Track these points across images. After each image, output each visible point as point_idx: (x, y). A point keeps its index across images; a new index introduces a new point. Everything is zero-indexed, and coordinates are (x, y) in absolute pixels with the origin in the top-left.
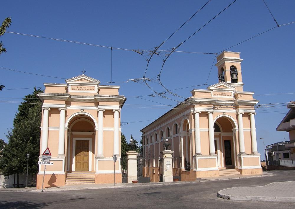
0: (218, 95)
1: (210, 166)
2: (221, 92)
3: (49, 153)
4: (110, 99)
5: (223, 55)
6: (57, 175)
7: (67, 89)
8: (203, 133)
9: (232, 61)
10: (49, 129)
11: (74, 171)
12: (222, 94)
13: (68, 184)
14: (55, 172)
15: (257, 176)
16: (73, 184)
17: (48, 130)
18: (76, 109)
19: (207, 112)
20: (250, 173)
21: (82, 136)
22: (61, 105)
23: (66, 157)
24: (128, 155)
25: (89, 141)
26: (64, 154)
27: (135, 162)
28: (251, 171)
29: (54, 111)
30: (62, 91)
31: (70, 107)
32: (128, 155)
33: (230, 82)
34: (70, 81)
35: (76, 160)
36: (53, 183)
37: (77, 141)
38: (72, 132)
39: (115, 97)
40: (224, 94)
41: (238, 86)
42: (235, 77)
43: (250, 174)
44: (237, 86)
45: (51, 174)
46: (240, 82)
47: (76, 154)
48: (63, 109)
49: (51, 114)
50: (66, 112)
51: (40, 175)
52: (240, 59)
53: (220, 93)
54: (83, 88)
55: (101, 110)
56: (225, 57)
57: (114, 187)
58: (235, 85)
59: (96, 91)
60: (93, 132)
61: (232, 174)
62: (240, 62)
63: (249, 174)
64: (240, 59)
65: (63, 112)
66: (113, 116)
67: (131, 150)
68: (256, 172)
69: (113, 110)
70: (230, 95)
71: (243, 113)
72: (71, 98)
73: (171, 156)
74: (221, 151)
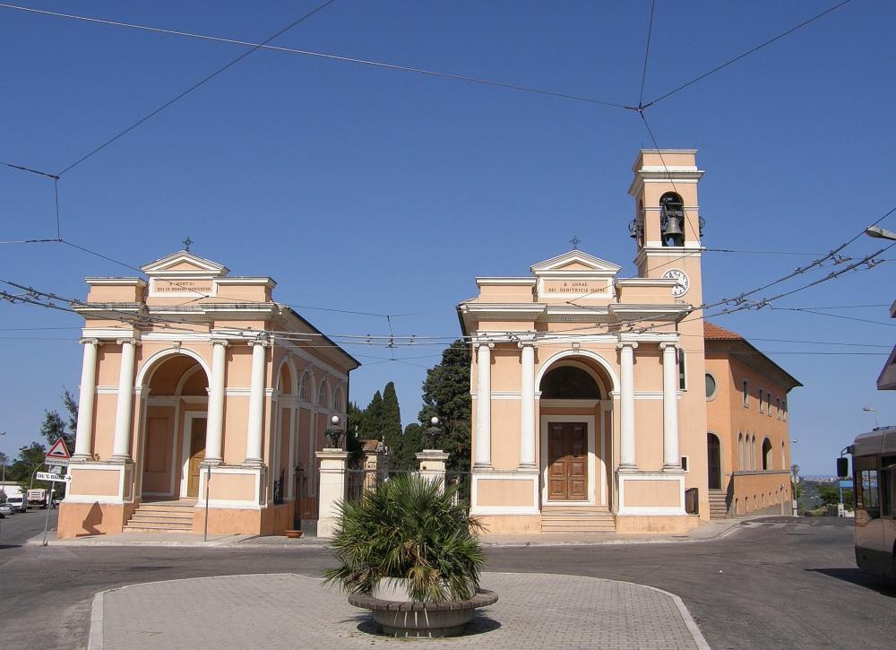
1: (514, 503)
2: (570, 282)
5: (640, 163)
6: (105, 505)
7: (143, 292)
8: (506, 408)
10: (228, 394)
11: (186, 496)
13: (129, 530)
14: (101, 499)
15: (631, 542)
16: (141, 530)
18: (160, 343)
19: (658, 344)
21: (573, 410)
24: (321, 459)
25: (549, 423)
27: (340, 479)
29: (106, 347)
30: (127, 295)
32: (321, 459)
33: (659, 244)
34: (152, 269)
36: (95, 527)
38: (183, 397)
39: (252, 308)
40: (582, 287)
42: (673, 228)
43: (646, 532)
44: (681, 255)
46: (692, 242)
48: (127, 342)
49: (233, 356)
50: (138, 349)
51: (66, 504)
52: (694, 169)
56: (645, 168)
58: (674, 253)
59: (609, 294)
60: (598, 401)
61: (583, 529)
62: (696, 181)
64: (694, 169)
65: (528, 354)
66: (518, 358)
67: (430, 448)
69: (118, 342)
71: (492, 345)
72: (151, 313)
74: (598, 455)
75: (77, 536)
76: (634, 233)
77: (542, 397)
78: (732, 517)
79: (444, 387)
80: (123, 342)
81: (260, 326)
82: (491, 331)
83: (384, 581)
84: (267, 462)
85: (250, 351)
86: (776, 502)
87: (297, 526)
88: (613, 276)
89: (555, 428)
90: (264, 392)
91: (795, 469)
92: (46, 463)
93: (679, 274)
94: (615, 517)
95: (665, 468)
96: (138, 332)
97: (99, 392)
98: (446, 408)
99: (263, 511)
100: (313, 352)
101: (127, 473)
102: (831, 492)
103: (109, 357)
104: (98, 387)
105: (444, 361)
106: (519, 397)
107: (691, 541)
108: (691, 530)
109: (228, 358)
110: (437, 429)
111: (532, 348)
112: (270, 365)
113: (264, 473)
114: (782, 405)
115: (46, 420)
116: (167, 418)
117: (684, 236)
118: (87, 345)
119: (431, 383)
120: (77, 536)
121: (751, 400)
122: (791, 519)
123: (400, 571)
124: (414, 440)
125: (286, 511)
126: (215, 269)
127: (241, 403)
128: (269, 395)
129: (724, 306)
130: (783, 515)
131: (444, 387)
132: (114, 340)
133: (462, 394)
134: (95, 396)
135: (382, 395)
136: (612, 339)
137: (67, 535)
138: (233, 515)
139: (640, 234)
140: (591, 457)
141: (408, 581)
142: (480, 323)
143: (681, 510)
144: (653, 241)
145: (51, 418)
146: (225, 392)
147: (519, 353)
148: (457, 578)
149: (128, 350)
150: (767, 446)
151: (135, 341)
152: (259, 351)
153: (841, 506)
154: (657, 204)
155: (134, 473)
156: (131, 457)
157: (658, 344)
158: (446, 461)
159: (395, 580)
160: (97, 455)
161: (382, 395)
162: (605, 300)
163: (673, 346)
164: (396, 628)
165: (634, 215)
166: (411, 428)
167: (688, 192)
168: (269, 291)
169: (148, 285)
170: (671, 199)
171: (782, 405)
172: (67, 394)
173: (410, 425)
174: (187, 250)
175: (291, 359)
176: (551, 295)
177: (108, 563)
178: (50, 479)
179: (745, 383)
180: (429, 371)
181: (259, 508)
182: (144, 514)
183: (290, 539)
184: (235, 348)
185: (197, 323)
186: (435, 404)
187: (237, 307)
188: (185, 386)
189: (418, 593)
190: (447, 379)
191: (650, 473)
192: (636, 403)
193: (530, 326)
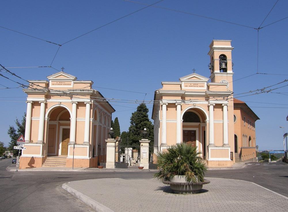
0: (190, 86)
2: (192, 83)
3: (23, 140)
4: (82, 93)
5: (212, 44)
7: (48, 85)
9: (222, 50)
10: (77, 120)
12: (194, 85)
14: (34, 156)
15: (215, 169)
16: (48, 166)
17: (76, 121)
18: (54, 102)
19: (222, 104)
20: (217, 165)
21: (193, 126)
22: (41, 98)
23: (91, 144)
24: (107, 142)
25: (63, 129)
26: (89, 141)
28: (219, 163)
29: (35, 104)
31: (50, 100)
32: (107, 142)
33: (219, 71)
34: (50, 78)
35: (62, 145)
37: (195, 131)
38: (59, 121)
41: (228, 75)
42: (224, 66)
43: (218, 166)
44: (226, 75)
45: (30, 157)
46: (230, 71)
47: (63, 141)
48: (42, 102)
50: (46, 105)
51: (22, 157)
52: (230, 47)
53: (192, 85)
54: (62, 84)
55: (74, 103)
56: (214, 46)
57: (71, 170)
58: (224, 75)
59: (205, 88)
60: (199, 123)
62: (231, 51)
63: (216, 166)
64: (230, 47)
65: (179, 107)
68: (224, 165)
69: (85, 103)
70: (203, 87)
71: (167, 104)
73: (148, 144)
74: (200, 141)
75: (26, 168)
76: (210, 68)
77: (183, 122)
78: (241, 161)
79: (138, 119)
80: (41, 103)
81: (89, 97)
82: (166, 100)
83: (176, 177)
84: (91, 143)
85: (85, 105)
86: (252, 157)
87: (99, 164)
88: (206, 82)
89: (185, 132)
90: (90, 119)
91: (257, 147)
92: (17, 143)
93: (225, 81)
94: (207, 161)
95: (224, 145)
96: (46, 99)
97: (33, 119)
98: (138, 126)
99: (90, 159)
100: (102, 105)
101: (43, 147)
102: (264, 155)
103: (36, 107)
104: (32, 118)
105: (138, 110)
106: (176, 122)
107: (234, 169)
108: (232, 165)
109: (77, 108)
110: (146, 132)
111: (213, 106)
112: (92, 110)
113: (90, 146)
114: (254, 126)
115: (9, 129)
116: (54, 128)
117: (227, 69)
118: (28, 103)
119: (133, 118)
120: (26, 168)
121: (246, 124)
122: (256, 163)
123: (183, 173)
124: (125, 137)
125: (96, 160)
126: (73, 78)
127: (82, 124)
128: (91, 120)
129: (258, 92)
130: (254, 162)
131: (138, 119)
132: (84, 102)
133: (144, 121)
134: (31, 121)
135: (114, 122)
136: (207, 103)
137: (22, 166)
138: (80, 161)
139: (212, 68)
140: (197, 142)
141: (184, 176)
142: (163, 97)
143: (229, 159)
144: (217, 70)
145: (11, 128)
146: (31, 118)
147: (176, 107)
148: (200, 175)
149: (43, 105)
150: (250, 139)
151: (45, 102)
152: (88, 106)
153: (270, 159)
154: (218, 58)
155: (45, 147)
156: (44, 141)
157: (222, 104)
158: (149, 143)
159: (180, 176)
160: (32, 141)
161: (114, 122)
162: (204, 90)
163: (227, 105)
164: (180, 191)
165: (209, 62)
166: (124, 133)
167: (229, 55)
168: (91, 86)
169: (49, 83)
170: (223, 57)
171: (254, 126)
172: (17, 120)
173: (123, 132)
174: (63, 71)
175: (97, 109)
176: (186, 88)
177: (48, 176)
178: (18, 149)
179: (244, 118)
180: (133, 114)
181: (89, 158)
182: (48, 161)
183: (100, 169)
184: (80, 104)
185: (82, 95)
186: (134, 124)
187: (81, 91)
188: (60, 117)
189: (189, 179)
190: (139, 116)
191: (219, 147)
192: (214, 124)
193: (180, 98)
